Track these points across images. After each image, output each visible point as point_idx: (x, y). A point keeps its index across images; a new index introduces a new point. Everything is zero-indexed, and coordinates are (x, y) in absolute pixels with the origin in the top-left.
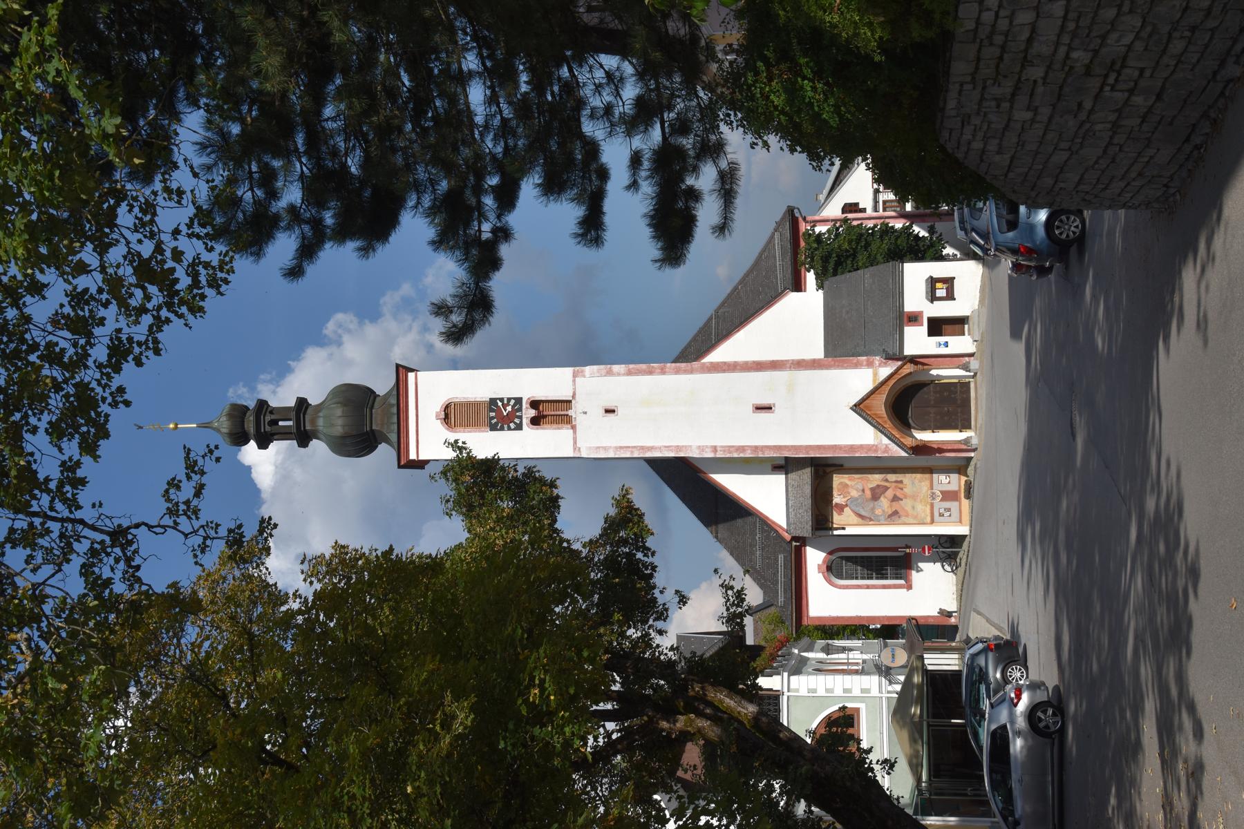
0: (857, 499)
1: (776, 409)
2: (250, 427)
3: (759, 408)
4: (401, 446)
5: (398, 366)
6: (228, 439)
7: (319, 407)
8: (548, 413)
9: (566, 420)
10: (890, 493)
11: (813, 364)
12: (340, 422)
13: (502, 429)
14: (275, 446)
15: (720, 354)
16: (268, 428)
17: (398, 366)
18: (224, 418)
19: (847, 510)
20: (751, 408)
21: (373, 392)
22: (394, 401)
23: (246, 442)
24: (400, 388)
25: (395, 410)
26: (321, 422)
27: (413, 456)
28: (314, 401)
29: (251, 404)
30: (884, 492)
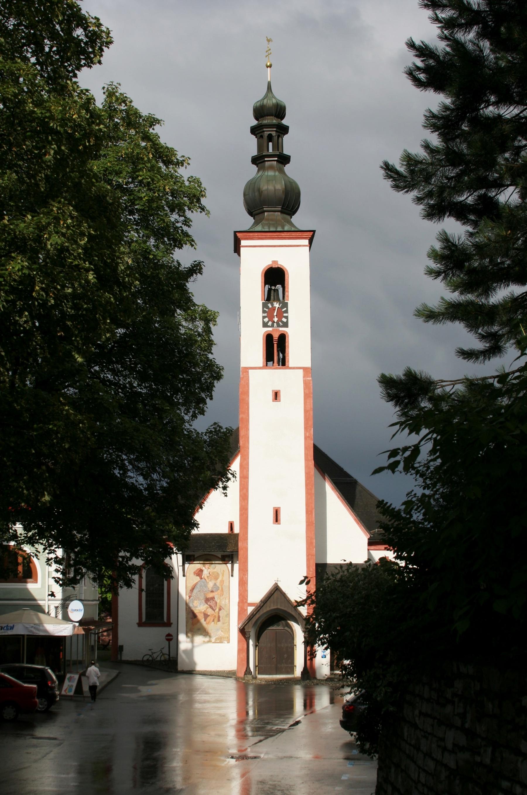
0: (206, 586)
1: (277, 526)
2: (266, 121)
3: (277, 513)
4: (250, 233)
5: (314, 232)
6: (258, 104)
7: (282, 172)
8: (276, 349)
9: (269, 357)
10: (210, 612)
11: (260, 368)
12: (271, 188)
13: (264, 312)
14: (253, 140)
15: (333, 501)
16: (266, 134)
17: (314, 232)
18: (274, 101)
19: (198, 578)
20: (277, 506)
21: (294, 213)
22: (286, 229)
23: (257, 118)
24: (297, 233)
25: (279, 229)
26: (271, 173)
27: (243, 243)
28: (287, 168)
29: (285, 122)
30: (211, 607)
